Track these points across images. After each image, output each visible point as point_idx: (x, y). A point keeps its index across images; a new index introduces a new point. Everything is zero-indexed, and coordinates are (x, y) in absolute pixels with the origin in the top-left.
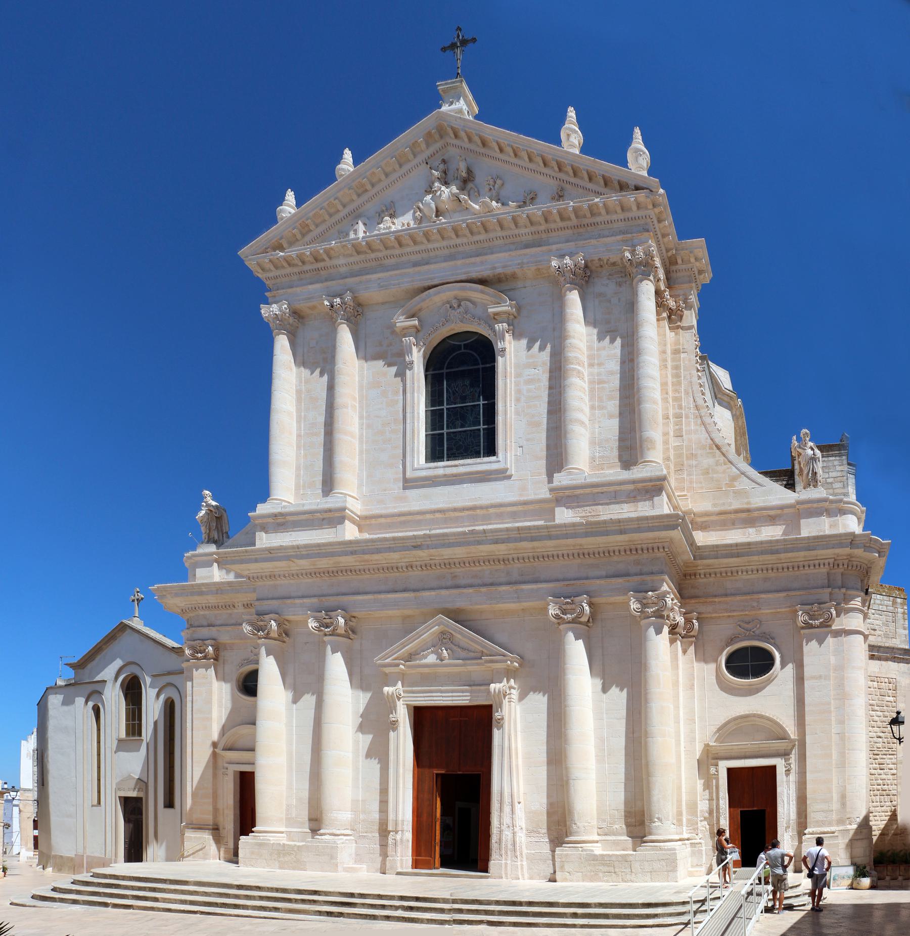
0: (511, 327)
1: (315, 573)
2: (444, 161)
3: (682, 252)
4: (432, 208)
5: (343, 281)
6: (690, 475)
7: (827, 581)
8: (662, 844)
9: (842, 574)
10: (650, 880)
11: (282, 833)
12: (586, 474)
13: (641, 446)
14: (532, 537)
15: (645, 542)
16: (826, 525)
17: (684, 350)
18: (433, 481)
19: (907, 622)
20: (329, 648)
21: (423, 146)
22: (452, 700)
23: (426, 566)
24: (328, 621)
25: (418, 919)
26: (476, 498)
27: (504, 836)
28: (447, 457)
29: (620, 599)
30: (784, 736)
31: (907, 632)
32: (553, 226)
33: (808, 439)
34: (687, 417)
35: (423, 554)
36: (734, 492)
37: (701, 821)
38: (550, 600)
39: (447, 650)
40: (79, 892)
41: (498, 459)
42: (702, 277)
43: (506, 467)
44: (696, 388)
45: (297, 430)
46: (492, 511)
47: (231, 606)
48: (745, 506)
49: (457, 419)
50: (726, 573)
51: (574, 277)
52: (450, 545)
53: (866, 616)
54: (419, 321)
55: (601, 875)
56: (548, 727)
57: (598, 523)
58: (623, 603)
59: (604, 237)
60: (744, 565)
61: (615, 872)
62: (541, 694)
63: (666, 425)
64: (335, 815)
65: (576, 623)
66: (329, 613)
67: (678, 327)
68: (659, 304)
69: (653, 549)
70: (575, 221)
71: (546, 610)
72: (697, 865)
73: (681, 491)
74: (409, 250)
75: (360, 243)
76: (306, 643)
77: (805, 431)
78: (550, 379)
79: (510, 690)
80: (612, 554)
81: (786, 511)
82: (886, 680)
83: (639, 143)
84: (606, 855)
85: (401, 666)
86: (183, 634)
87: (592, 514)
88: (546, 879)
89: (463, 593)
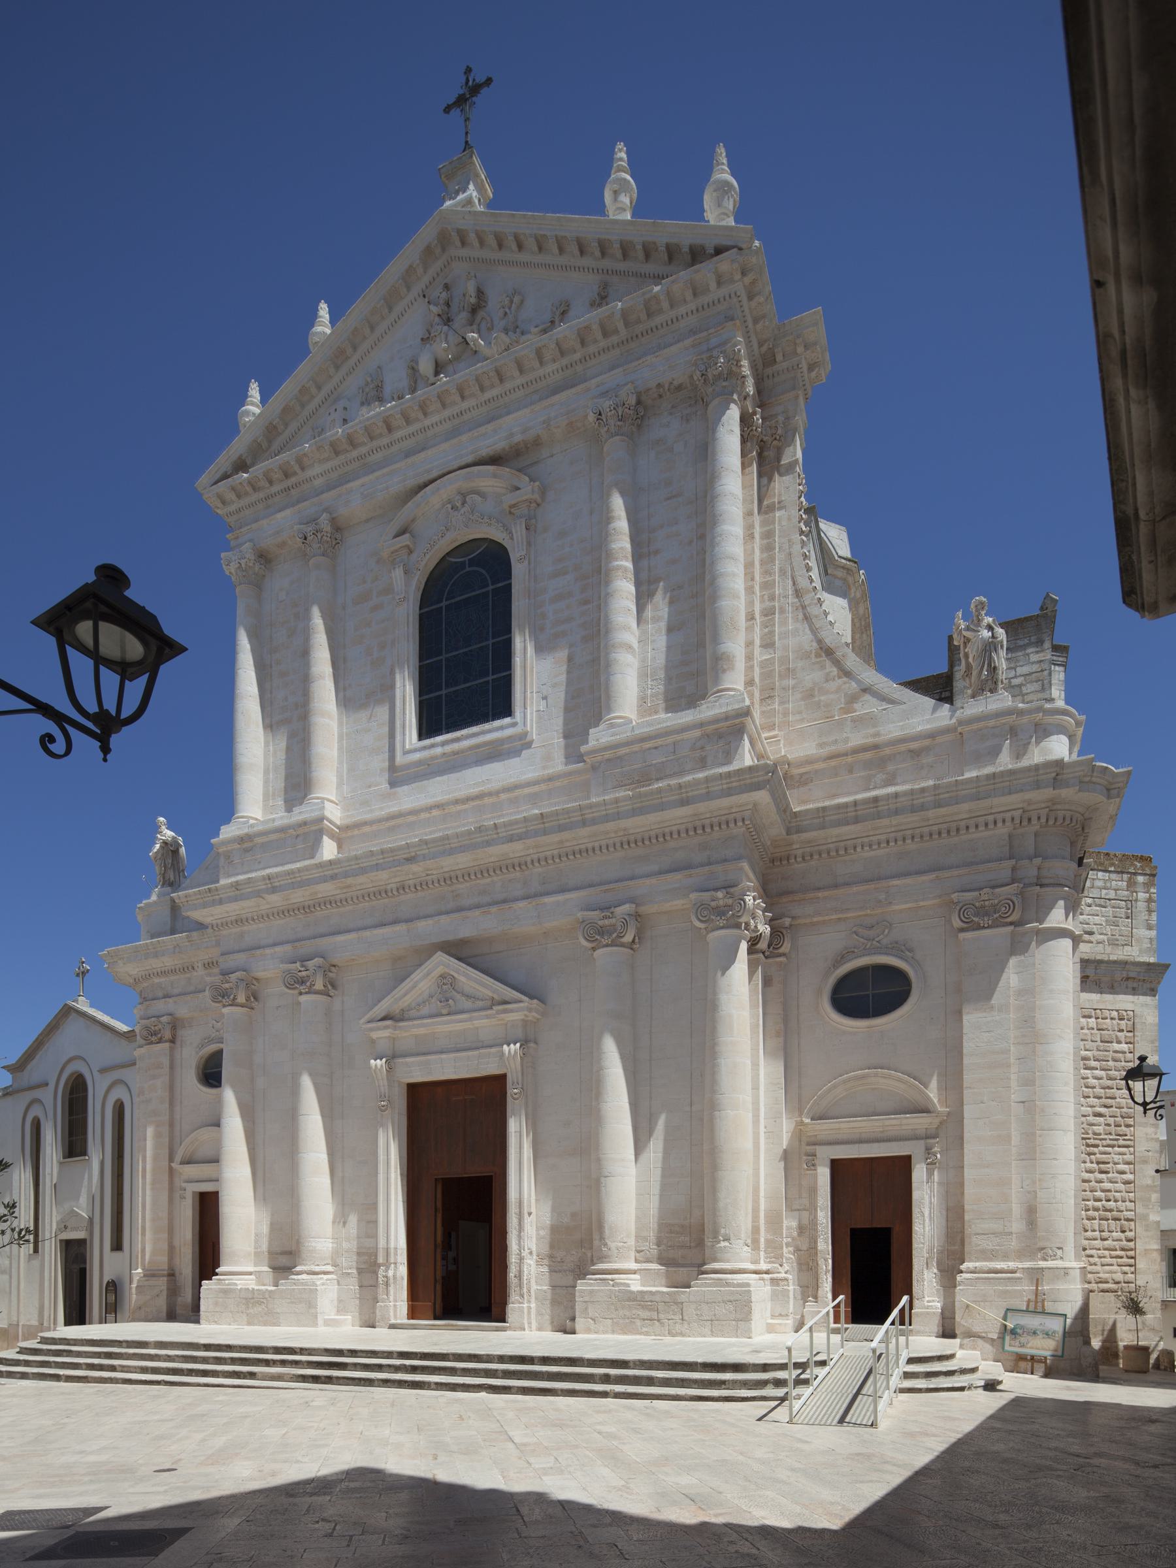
1: (288, 911)
5: (317, 498)
9: (1036, 834)
10: (710, 1333)
11: (250, 1274)
14: (559, 826)
18: (428, 765)
19: (1154, 916)
21: (420, 270)
23: (422, 885)
24: (304, 974)
27: (525, 1267)
31: (1153, 933)
33: (983, 613)
34: (782, 611)
40: (27, 1363)
41: (514, 720)
44: (798, 561)
46: (503, 796)
47: (190, 968)
48: (870, 740)
50: (837, 851)
52: (451, 852)
55: (638, 1323)
60: (865, 835)
61: (658, 1321)
63: (750, 629)
64: (313, 1244)
65: (616, 946)
66: (305, 963)
68: (746, 437)
70: (623, 333)
72: (780, 1315)
73: (770, 730)
76: (277, 1008)
80: (668, 838)
82: (1115, 1014)
86: (135, 1011)
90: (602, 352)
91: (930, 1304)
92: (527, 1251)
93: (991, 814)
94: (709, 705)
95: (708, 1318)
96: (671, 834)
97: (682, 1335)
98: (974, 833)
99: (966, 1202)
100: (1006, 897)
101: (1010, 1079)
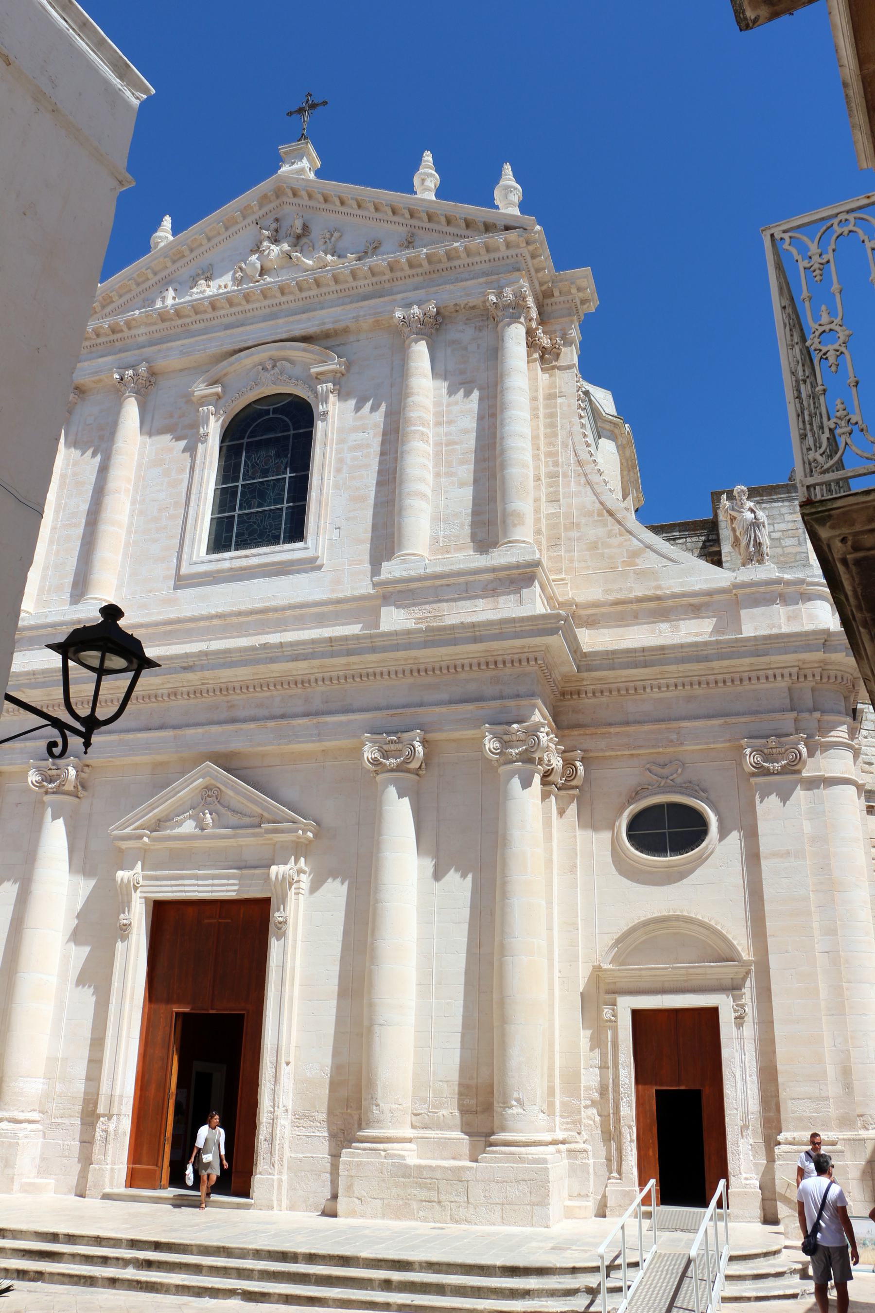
0: (337, 387)
2: (277, 220)
3: (560, 284)
4: (256, 268)
6: (570, 551)
7: (788, 701)
8: (523, 1149)
9: (813, 690)
10: (500, 1220)
12: (427, 561)
13: (504, 522)
15: (509, 652)
16: (782, 617)
17: (562, 394)
18: (214, 577)
20: (49, 811)
21: (256, 208)
22: (212, 892)
23: (196, 693)
24: (54, 772)
25: (161, 1284)
26: (269, 597)
27: (279, 1128)
28: (236, 545)
29: (470, 733)
30: (729, 956)
32: (399, 274)
33: (744, 498)
34: (565, 475)
35: (192, 677)
36: (636, 573)
37: (586, 1107)
38: (367, 737)
39: (211, 814)
41: (306, 546)
42: (585, 306)
43: (316, 555)
45: (53, 522)
46: (288, 613)
48: (653, 592)
49: (254, 497)
50: (627, 690)
51: (422, 327)
52: (233, 665)
53: (856, 753)
54: (223, 387)
55: (415, 1205)
56: (346, 933)
57: (444, 628)
58: (473, 739)
59: (462, 281)
61: (439, 1202)
62: (339, 880)
63: (537, 488)
65: (402, 771)
67: (553, 368)
68: (529, 344)
69: (520, 661)
71: (358, 751)
72: (579, 1195)
73: (556, 574)
74: (222, 312)
75: (168, 312)
76: (17, 805)
77: (739, 488)
78: (383, 443)
79: (298, 875)
80: (459, 670)
81: (717, 597)
83: (510, 180)
84: (425, 1167)
85: (146, 839)
87: (433, 614)
88: (316, 1210)
89: (241, 729)
90: (407, 278)
91: (748, 1182)
92: (282, 1109)
93: (771, 669)
94: (502, 553)
95: (498, 1201)
96: (463, 666)
97: (467, 1221)
98: (755, 684)
99: (778, 1063)
100: (792, 746)
101: (812, 928)
